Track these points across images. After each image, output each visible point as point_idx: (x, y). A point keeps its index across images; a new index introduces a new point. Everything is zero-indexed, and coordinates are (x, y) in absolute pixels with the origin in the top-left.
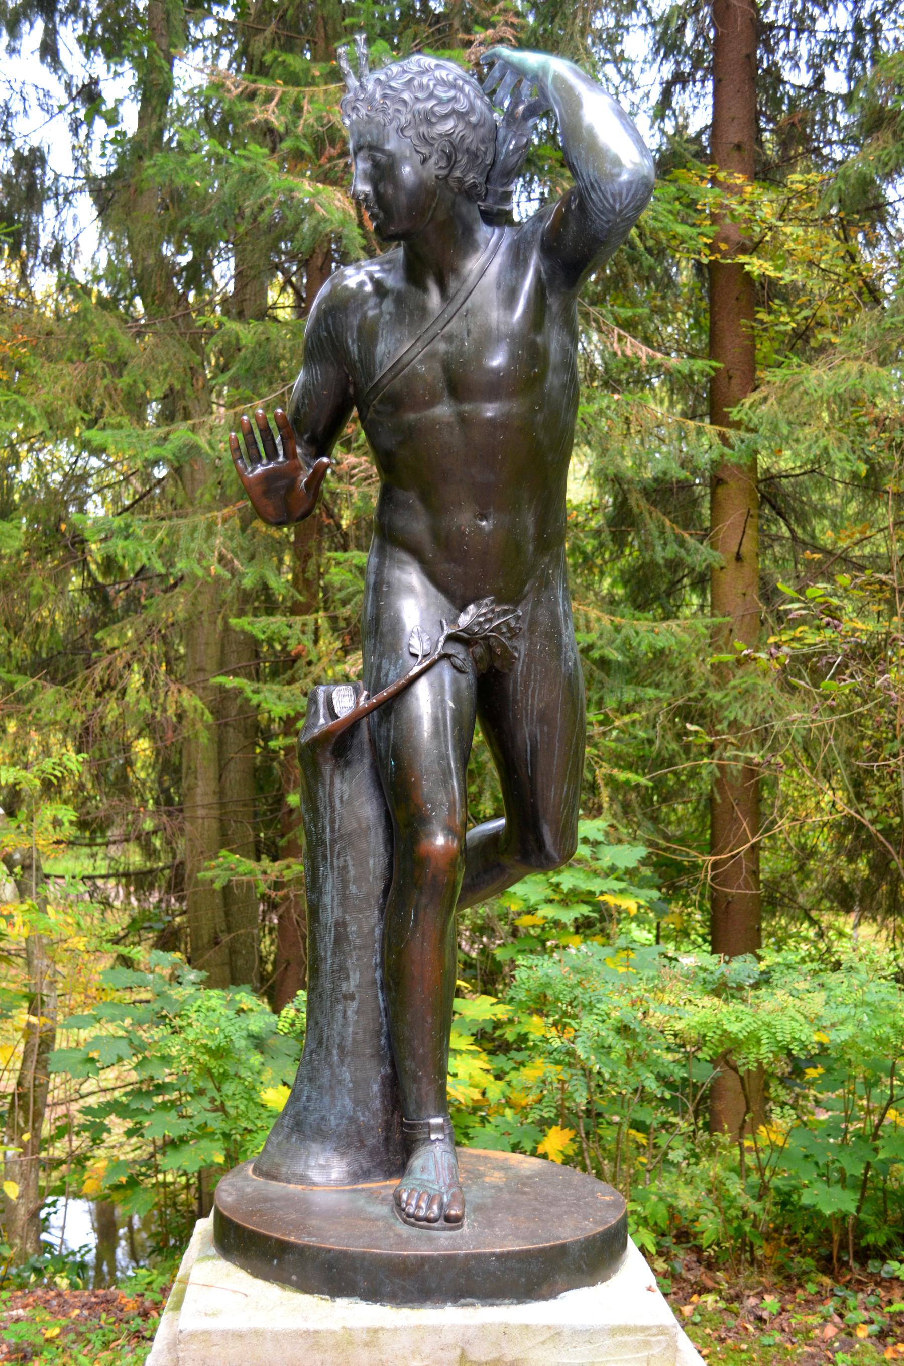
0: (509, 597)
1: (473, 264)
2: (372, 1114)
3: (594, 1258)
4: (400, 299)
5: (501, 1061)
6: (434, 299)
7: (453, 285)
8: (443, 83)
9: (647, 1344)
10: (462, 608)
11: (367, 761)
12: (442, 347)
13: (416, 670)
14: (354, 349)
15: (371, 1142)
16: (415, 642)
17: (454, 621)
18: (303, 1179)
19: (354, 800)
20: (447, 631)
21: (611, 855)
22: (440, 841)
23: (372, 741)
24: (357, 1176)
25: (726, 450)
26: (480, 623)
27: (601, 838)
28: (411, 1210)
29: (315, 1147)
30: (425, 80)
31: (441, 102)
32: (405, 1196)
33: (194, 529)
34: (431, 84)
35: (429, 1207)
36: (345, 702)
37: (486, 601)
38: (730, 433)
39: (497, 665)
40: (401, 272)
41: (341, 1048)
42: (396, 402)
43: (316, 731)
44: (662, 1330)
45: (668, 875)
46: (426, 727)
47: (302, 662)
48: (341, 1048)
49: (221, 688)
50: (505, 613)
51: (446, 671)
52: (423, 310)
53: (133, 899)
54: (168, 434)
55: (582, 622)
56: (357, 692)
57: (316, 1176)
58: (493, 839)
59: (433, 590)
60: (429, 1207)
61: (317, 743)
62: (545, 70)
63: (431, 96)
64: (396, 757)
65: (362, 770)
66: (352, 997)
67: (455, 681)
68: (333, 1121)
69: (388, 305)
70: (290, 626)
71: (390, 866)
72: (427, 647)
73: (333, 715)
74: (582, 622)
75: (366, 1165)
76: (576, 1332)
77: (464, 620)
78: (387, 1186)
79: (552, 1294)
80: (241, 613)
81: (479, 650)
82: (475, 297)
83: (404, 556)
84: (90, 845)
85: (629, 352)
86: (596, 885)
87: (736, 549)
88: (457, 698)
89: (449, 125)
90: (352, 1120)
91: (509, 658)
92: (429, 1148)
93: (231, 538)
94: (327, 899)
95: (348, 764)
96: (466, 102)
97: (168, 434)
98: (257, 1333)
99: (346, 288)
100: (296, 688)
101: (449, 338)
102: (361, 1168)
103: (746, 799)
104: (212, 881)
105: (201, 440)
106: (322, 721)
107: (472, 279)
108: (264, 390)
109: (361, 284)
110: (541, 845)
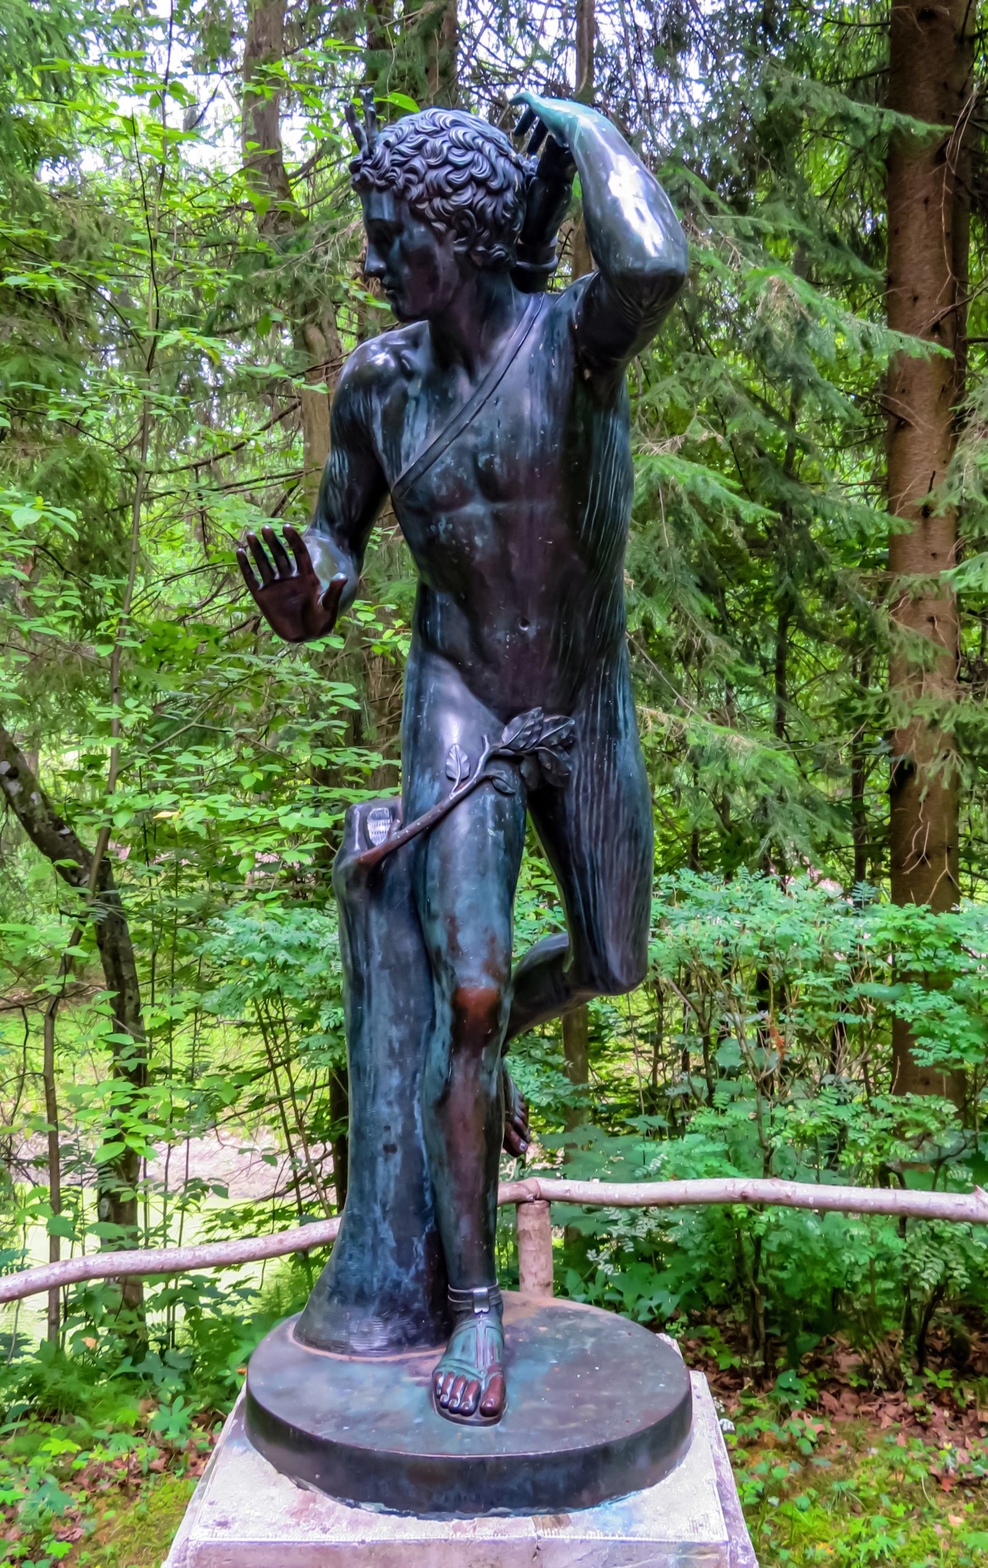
1: (504, 344)
8: (457, 145)
10: (506, 720)
26: (527, 738)
28: (445, 1399)
30: (438, 142)
31: (457, 168)
32: (441, 1381)
34: (445, 146)
35: (464, 1398)
36: (380, 831)
37: (533, 712)
50: (556, 723)
60: (464, 1398)
62: (573, 124)
63: (446, 162)
73: (370, 845)
77: (507, 736)
78: (427, 1359)
83: (443, 664)
89: (466, 196)
92: (472, 1322)
96: (486, 166)
99: (371, 366)
102: (405, 1334)
106: (357, 847)
109: (386, 362)
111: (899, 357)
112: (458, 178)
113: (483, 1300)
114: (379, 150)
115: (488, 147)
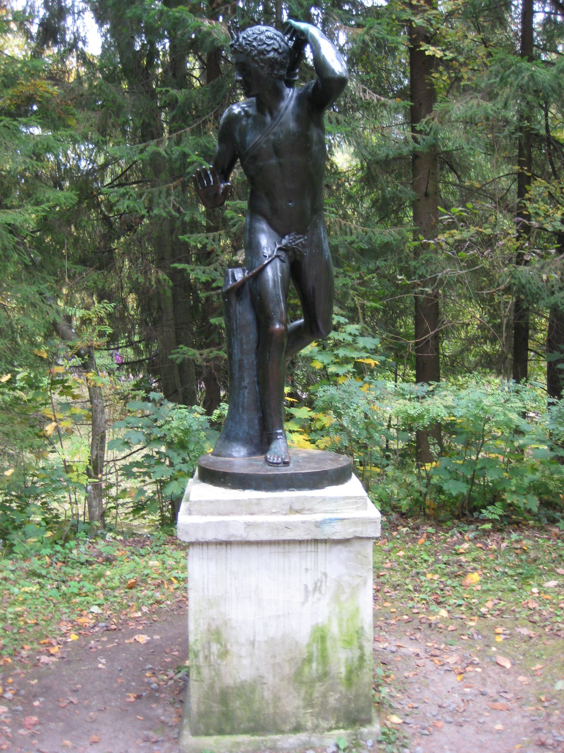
0: (302, 231)
2: (255, 431)
3: (339, 477)
4: (255, 118)
5: (313, 436)
6: (268, 119)
7: (275, 113)
8: (268, 37)
9: (356, 503)
10: (283, 237)
11: (248, 297)
12: (272, 137)
13: (266, 262)
14: (238, 138)
15: (255, 441)
16: (265, 251)
17: (280, 243)
18: (230, 456)
19: (244, 313)
20: (278, 246)
21: (361, 342)
22: (277, 326)
23: (250, 290)
24: (250, 454)
25: (416, 145)
27: (357, 333)
29: (234, 444)
30: (262, 37)
31: (268, 45)
33: (160, 193)
38: (418, 136)
39: (298, 258)
40: (255, 108)
41: (243, 407)
42: (255, 158)
43: (229, 287)
44: (362, 498)
45: (395, 351)
46: (271, 283)
47: (213, 255)
48: (243, 407)
49: (175, 268)
50: (300, 238)
51: (278, 262)
52: (264, 123)
53: (131, 375)
54: (145, 147)
55: (348, 230)
56: (244, 271)
57: (235, 454)
58: (299, 327)
59: (272, 231)
61: (229, 292)
63: (265, 43)
64: (260, 295)
65: (247, 301)
66: (246, 388)
67: (281, 266)
68: (241, 434)
69: (250, 121)
70: (207, 238)
71: (259, 338)
72: (270, 252)
74: (348, 230)
75: (254, 450)
76: (331, 499)
77: (284, 242)
79: (322, 487)
80: (184, 233)
81: (290, 253)
82: (284, 118)
83: (260, 218)
84: (107, 350)
85: (368, 97)
86: (355, 355)
87: (424, 190)
88: (282, 272)
90: (248, 434)
91: (302, 255)
93: (178, 197)
94: (235, 351)
95: (241, 299)
97: (145, 147)
98: (218, 501)
99: (234, 114)
100: (212, 267)
101: (275, 134)
103: (429, 313)
104: (176, 359)
105: (161, 150)
107: (282, 110)
108: (191, 122)
109: (240, 112)
110: (318, 329)
111: (415, 246)
112: (269, 49)
113: (281, 434)
114: (241, 40)
115: (278, 38)
